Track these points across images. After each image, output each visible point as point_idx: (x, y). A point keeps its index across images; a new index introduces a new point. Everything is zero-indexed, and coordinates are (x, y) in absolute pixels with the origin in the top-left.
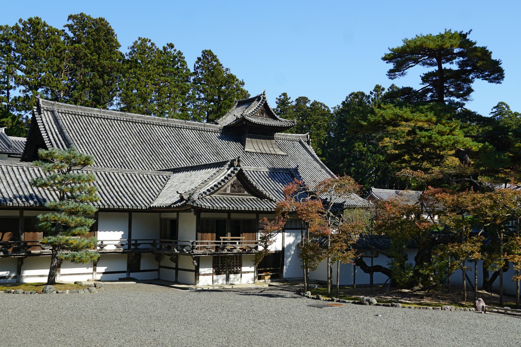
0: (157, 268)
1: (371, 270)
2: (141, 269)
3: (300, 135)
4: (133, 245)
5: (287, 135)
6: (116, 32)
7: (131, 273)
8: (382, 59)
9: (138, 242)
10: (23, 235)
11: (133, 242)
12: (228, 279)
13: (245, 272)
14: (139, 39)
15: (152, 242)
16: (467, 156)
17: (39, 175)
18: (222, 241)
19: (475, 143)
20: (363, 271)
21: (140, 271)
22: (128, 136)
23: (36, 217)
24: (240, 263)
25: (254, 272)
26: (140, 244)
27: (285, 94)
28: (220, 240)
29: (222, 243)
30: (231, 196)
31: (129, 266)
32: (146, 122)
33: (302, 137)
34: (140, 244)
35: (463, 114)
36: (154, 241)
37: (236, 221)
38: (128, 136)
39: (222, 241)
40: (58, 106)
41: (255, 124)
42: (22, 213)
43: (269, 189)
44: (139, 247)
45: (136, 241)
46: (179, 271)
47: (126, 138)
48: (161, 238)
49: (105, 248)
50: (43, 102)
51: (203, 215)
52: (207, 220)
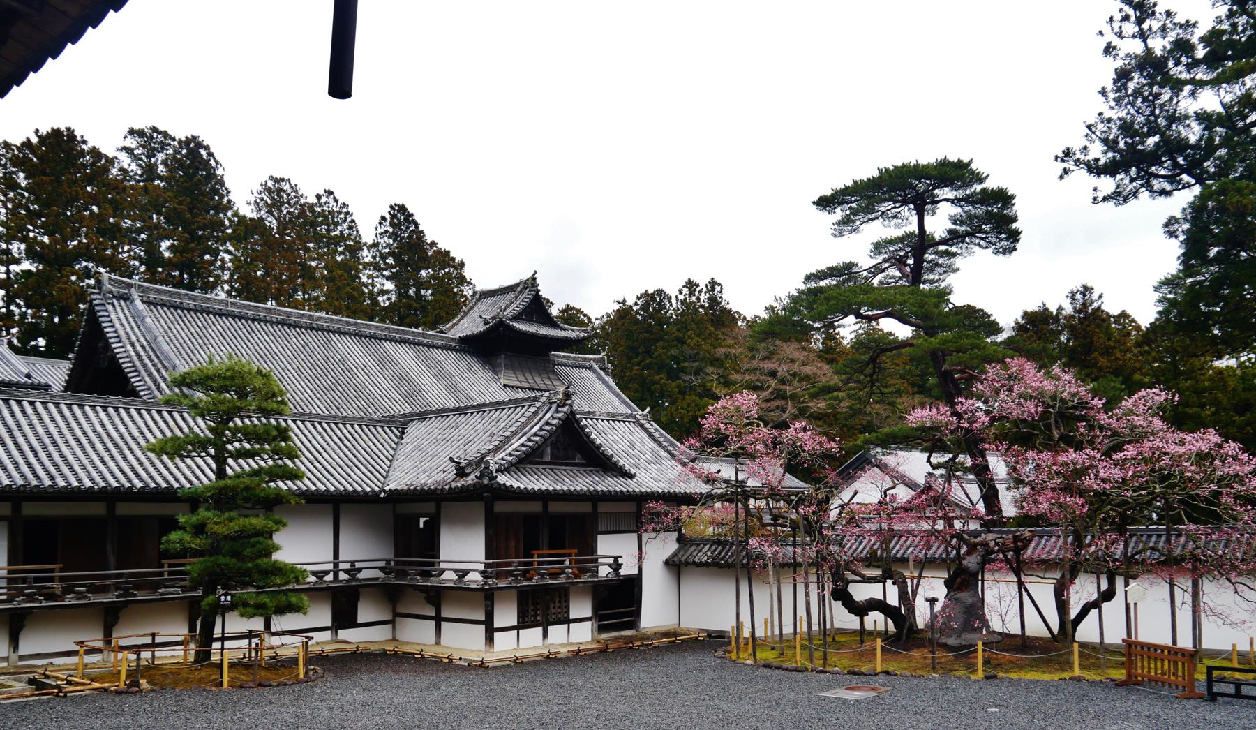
0: (389, 617)
1: (860, 610)
2: (360, 621)
3: (591, 356)
5: (570, 357)
7: (339, 631)
8: (1014, 236)
9: (358, 565)
12: (545, 635)
15: (382, 564)
17: (186, 430)
18: (166, 569)
20: (846, 610)
22: (283, 352)
23: (174, 516)
24: (565, 601)
26: (360, 570)
27: (1086, 289)
28: (162, 566)
29: (166, 574)
30: (552, 467)
32: (315, 326)
33: (595, 360)
34: (360, 570)
36: (388, 561)
37: (561, 518)
38: (283, 352)
39: (166, 569)
40: (141, 289)
41: (521, 332)
42: (111, 509)
45: (353, 563)
46: (444, 624)
47: (282, 357)
48: (9, 564)
50: (110, 279)
51: (500, 507)
52: (508, 517)
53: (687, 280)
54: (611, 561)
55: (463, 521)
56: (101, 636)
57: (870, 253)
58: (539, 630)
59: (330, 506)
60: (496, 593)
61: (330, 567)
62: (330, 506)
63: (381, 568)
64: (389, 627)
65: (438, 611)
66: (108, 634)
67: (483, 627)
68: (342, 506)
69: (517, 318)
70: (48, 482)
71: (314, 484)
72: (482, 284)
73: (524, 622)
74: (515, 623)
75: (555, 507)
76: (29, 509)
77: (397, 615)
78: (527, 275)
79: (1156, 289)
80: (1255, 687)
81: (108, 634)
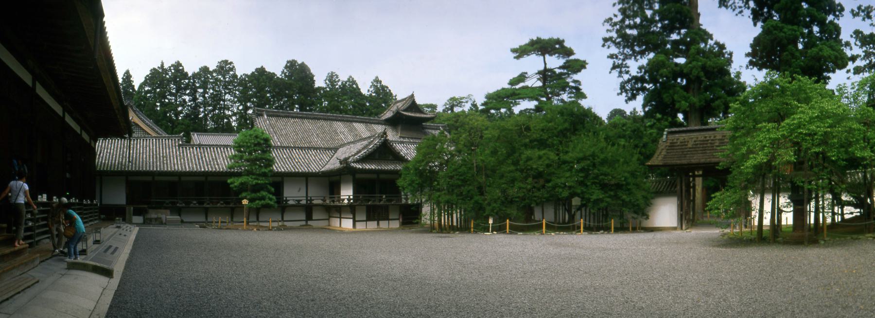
0: (327, 218)
2: (313, 218)
4: (309, 200)
6: (622, 109)
9: (288, 199)
10: (813, 204)
11: (309, 198)
12: (378, 224)
13: (392, 220)
14: (325, 80)
15: (322, 198)
16: (424, 124)
19: (819, 148)
21: (312, 220)
25: (340, 218)
26: (289, 200)
31: (367, 218)
34: (313, 200)
35: (325, 92)
36: (349, 196)
41: (405, 115)
43: (161, 146)
44: (301, 202)
45: (311, 197)
49: (288, 202)
51: (358, 176)
53: (374, 78)
54: (348, 197)
55: (347, 182)
56: (204, 217)
57: (629, 69)
58: (376, 222)
59: (304, 179)
60: (314, 208)
61: (305, 198)
62: (304, 178)
63: (322, 200)
64: (327, 221)
65: (340, 215)
66: (232, 218)
67: (352, 220)
68: (309, 178)
69: (406, 110)
70: (210, 169)
71: (280, 168)
72: (399, 98)
73: (369, 219)
74: (365, 219)
75: (382, 176)
76: (131, 178)
77: (330, 217)
78: (410, 94)
79: (731, 54)
80: (87, 317)
81: (232, 218)
